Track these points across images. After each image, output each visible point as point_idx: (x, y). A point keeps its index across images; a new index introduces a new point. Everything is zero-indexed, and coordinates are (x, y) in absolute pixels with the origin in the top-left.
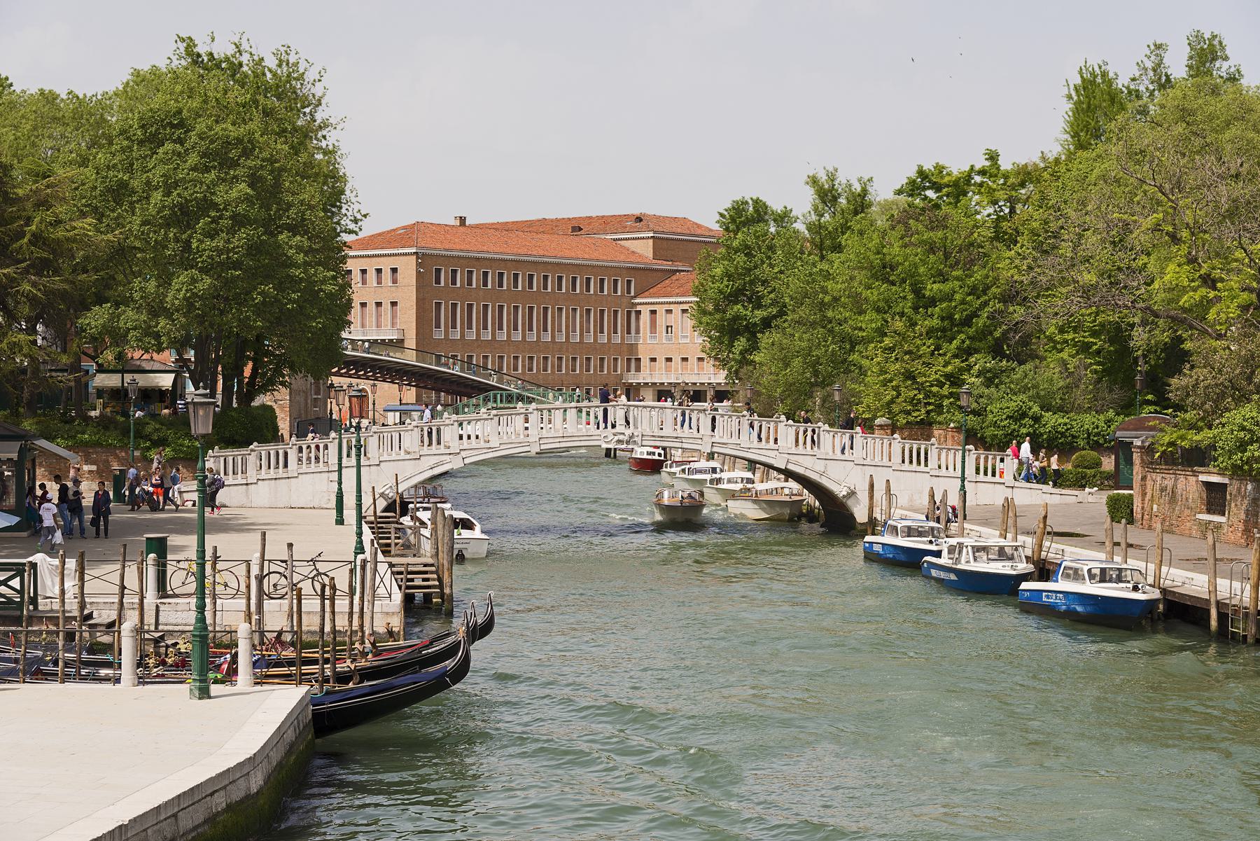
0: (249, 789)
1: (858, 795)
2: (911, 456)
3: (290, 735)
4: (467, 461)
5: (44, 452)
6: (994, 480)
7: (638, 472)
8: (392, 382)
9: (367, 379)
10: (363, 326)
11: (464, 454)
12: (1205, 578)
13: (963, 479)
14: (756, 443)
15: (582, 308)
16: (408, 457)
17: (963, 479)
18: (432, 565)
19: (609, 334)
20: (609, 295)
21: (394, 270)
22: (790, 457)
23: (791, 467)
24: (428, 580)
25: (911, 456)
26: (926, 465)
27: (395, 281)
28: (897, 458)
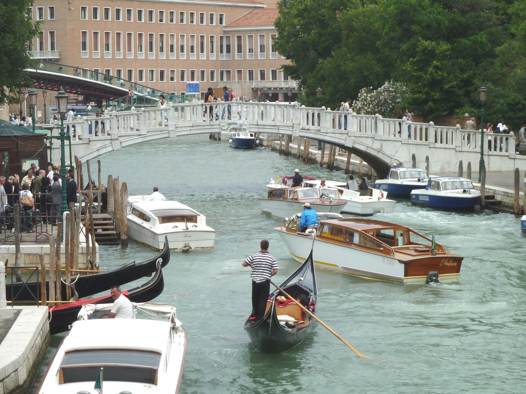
0: (17, 380)
1: (367, 384)
2: (415, 132)
3: (39, 341)
4: (124, 144)
5: (507, 186)
6: (501, 153)
7: (237, 148)
8: (52, 90)
9: (41, 88)
10: (41, 49)
11: (121, 139)
12: (14, 246)
13: (482, 154)
14: (331, 130)
15: (188, 35)
16: (81, 142)
17: (482, 154)
18: (110, 219)
19: (207, 54)
20: (207, 25)
21: (52, 9)
22: (356, 139)
23: (358, 146)
24: (108, 230)
25: (415, 132)
26: (426, 140)
27: (52, 16)
28: (432, 139)
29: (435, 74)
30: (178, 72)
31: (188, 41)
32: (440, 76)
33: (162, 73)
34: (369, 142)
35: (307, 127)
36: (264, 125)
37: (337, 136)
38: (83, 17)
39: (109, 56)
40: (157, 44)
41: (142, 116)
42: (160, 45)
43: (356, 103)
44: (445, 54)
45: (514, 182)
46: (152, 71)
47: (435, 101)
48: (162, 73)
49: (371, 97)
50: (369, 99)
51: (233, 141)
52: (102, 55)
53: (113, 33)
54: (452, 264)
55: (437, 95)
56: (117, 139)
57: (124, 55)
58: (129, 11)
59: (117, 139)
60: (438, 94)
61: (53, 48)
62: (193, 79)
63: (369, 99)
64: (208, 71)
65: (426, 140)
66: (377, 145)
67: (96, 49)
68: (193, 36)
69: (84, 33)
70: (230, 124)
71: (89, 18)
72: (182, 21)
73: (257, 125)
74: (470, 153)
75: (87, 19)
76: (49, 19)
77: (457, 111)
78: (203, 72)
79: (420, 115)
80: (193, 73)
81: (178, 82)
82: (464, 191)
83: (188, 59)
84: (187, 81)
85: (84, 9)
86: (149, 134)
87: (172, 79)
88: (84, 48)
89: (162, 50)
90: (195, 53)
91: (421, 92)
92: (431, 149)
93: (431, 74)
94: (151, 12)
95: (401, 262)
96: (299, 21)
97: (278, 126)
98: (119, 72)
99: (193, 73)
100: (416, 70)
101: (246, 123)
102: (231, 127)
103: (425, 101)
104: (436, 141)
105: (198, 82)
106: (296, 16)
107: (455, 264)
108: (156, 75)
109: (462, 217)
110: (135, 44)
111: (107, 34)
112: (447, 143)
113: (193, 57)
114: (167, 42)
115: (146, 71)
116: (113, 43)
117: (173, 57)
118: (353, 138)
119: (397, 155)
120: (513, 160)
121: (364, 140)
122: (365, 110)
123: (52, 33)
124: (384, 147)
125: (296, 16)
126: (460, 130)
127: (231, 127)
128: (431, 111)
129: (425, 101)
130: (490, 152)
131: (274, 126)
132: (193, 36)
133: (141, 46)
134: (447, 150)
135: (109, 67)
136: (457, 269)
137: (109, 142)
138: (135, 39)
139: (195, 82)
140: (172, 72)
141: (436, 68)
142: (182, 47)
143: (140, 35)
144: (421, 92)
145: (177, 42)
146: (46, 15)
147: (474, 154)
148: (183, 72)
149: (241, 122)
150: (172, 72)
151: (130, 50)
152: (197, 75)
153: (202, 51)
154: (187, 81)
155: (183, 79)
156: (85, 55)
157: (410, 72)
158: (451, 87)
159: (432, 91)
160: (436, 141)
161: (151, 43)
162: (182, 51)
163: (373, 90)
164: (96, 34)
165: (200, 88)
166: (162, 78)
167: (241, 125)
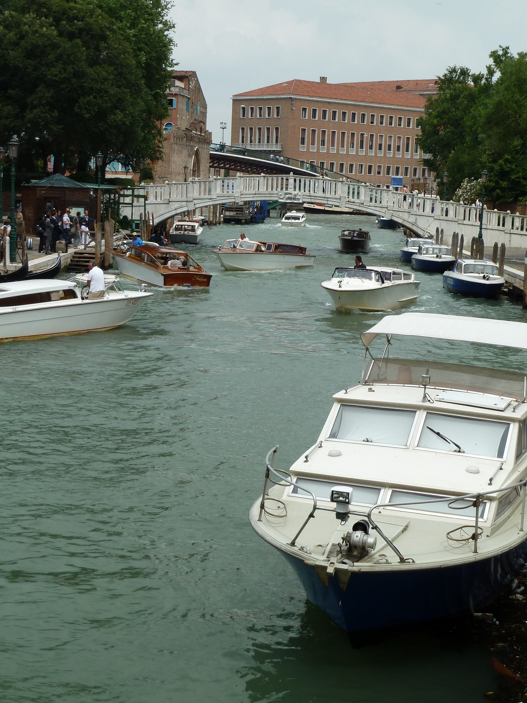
7: (382, 228)
10: (268, 142)
11: (195, 201)
20: (413, 129)
21: (278, 108)
22: (395, 212)
26: (503, 225)
29: (504, 166)
30: (384, 168)
31: (395, 141)
32: (509, 167)
33: (370, 167)
34: (405, 216)
35: (353, 200)
36: (316, 197)
37: (378, 209)
38: (304, 116)
39: (323, 150)
40: (367, 143)
41: (214, 183)
42: (369, 143)
43: (459, 191)
44: (515, 148)
45: (492, 252)
46: (362, 165)
47: (503, 189)
48: (370, 167)
49: (470, 186)
50: (468, 188)
51: (379, 222)
52: (318, 149)
53: (329, 131)
54: (203, 280)
55: (504, 184)
56: (192, 201)
57: (338, 150)
58: (344, 113)
59: (192, 201)
60: (505, 183)
61: (277, 142)
62: (397, 174)
63: (468, 188)
64: (411, 168)
65: (503, 225)
66: (412, 219)
67: (313, 144)
68: (399, 138)
69: (304, 130)
70: (286, 194)
71: (309, 117)
72: (391, 124)
73: (310, 196)
74: (494, 231)
75: (307, 118)
76: (275, 117)
77: (520, 198)
78: (407, 169)
79: (490, 201)
80: (398, 169)
81: (384, 176)
82: (437, 257)
83: (394, 157)
84: (392, 175)
85: (304, 109)
86: (218, 198)
87: (379, 173)
88: (303, 142)
89: (371, 148)
90: (401, 152)
91: (492, 181)
92: (460, 225)
93: (501, 165)
94: (363, 115)
95: (162, 275)
96: (438, 121)
97: (328, 198)
98: (332, 164)
99: (398, 169)
100: (491, 162)
101: (300, 194)
102: (287, 196)
103: (494, 189)
104: (464, 219)
105: (402, 177)
106: (436, 117)
107: (205, 280)
108: (365, 169)
109: (428, 277)
110: (348, 142)
111: (324, 132)
112: (469, 220)
113: (399, 155)
114: (376, 141)
115: (356, 165)
116: (328, 140)
117: (381, 154)
118: (392, 212)
119: (429, 228)
120: (509, 235)
121: (401, 214)
122: (464, 197)
123: (277, 129)
124: (418, 220)
125: (436, 117)
126: (487, 210)
127: (287, 196)
128: (499, 197)
129: (494, 189)
130: (512, 230)
131: (325, 198)
132: (399, 138)
133: (353, 144)
134: (473, 227)
135: (323, 160)
136: (207, 284)
137: (184, 203)
138: (348, 138)
139: (399, 177)
140: (380, 167)
141: (507, 160)
142: (390, 146)
143: (353, 134)
144: (492, 181)
145: (386, 142)
146: (273, 114)
147: (497, 231)
148: (389, 168)
149: (296, 193)
150: (380, 167)
151: (343, 146)
152: (402, 170)
153: (407, 150)
154: (392, 175)
155: (388, 173)
156: (303, 149)
157: (485, 163)
158: (517, 178)
159: (501, 180)
160: (464, 219)
161: (362, 142)
162: (389, 149)
163: (474, 180)
164: (314, 131)
165: (403, 182)
166: (370, 172)
167: (296, 195)
